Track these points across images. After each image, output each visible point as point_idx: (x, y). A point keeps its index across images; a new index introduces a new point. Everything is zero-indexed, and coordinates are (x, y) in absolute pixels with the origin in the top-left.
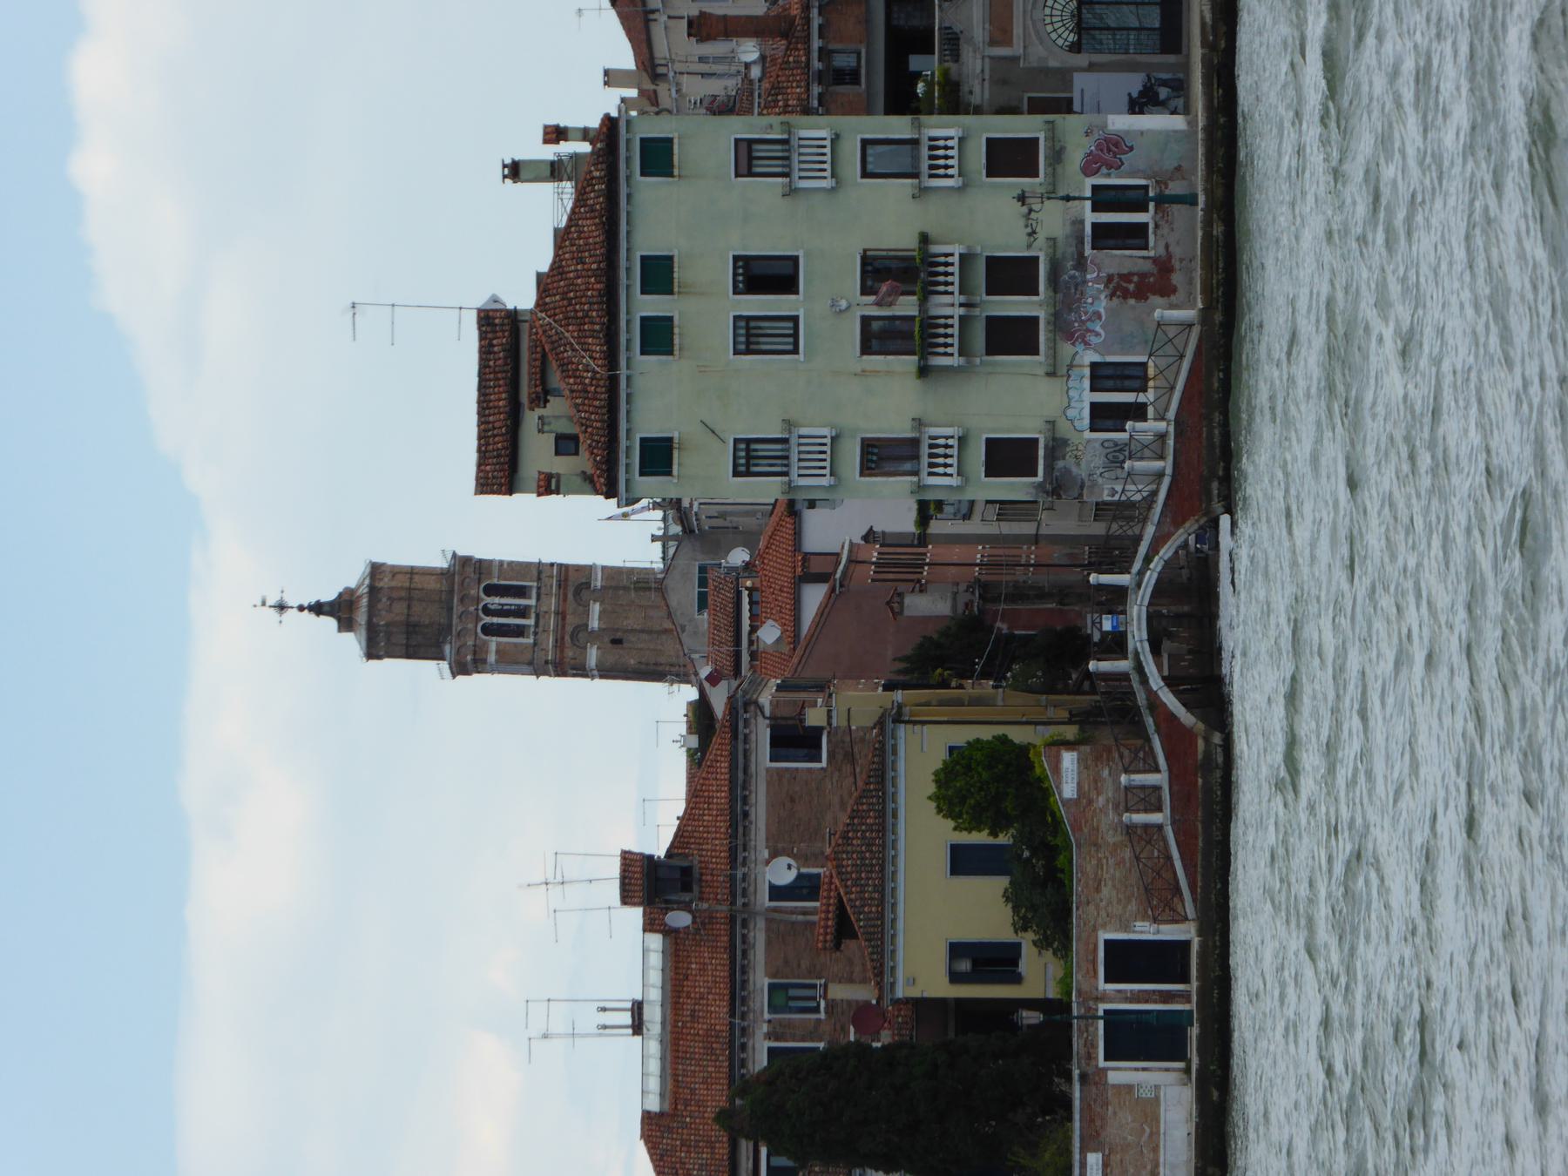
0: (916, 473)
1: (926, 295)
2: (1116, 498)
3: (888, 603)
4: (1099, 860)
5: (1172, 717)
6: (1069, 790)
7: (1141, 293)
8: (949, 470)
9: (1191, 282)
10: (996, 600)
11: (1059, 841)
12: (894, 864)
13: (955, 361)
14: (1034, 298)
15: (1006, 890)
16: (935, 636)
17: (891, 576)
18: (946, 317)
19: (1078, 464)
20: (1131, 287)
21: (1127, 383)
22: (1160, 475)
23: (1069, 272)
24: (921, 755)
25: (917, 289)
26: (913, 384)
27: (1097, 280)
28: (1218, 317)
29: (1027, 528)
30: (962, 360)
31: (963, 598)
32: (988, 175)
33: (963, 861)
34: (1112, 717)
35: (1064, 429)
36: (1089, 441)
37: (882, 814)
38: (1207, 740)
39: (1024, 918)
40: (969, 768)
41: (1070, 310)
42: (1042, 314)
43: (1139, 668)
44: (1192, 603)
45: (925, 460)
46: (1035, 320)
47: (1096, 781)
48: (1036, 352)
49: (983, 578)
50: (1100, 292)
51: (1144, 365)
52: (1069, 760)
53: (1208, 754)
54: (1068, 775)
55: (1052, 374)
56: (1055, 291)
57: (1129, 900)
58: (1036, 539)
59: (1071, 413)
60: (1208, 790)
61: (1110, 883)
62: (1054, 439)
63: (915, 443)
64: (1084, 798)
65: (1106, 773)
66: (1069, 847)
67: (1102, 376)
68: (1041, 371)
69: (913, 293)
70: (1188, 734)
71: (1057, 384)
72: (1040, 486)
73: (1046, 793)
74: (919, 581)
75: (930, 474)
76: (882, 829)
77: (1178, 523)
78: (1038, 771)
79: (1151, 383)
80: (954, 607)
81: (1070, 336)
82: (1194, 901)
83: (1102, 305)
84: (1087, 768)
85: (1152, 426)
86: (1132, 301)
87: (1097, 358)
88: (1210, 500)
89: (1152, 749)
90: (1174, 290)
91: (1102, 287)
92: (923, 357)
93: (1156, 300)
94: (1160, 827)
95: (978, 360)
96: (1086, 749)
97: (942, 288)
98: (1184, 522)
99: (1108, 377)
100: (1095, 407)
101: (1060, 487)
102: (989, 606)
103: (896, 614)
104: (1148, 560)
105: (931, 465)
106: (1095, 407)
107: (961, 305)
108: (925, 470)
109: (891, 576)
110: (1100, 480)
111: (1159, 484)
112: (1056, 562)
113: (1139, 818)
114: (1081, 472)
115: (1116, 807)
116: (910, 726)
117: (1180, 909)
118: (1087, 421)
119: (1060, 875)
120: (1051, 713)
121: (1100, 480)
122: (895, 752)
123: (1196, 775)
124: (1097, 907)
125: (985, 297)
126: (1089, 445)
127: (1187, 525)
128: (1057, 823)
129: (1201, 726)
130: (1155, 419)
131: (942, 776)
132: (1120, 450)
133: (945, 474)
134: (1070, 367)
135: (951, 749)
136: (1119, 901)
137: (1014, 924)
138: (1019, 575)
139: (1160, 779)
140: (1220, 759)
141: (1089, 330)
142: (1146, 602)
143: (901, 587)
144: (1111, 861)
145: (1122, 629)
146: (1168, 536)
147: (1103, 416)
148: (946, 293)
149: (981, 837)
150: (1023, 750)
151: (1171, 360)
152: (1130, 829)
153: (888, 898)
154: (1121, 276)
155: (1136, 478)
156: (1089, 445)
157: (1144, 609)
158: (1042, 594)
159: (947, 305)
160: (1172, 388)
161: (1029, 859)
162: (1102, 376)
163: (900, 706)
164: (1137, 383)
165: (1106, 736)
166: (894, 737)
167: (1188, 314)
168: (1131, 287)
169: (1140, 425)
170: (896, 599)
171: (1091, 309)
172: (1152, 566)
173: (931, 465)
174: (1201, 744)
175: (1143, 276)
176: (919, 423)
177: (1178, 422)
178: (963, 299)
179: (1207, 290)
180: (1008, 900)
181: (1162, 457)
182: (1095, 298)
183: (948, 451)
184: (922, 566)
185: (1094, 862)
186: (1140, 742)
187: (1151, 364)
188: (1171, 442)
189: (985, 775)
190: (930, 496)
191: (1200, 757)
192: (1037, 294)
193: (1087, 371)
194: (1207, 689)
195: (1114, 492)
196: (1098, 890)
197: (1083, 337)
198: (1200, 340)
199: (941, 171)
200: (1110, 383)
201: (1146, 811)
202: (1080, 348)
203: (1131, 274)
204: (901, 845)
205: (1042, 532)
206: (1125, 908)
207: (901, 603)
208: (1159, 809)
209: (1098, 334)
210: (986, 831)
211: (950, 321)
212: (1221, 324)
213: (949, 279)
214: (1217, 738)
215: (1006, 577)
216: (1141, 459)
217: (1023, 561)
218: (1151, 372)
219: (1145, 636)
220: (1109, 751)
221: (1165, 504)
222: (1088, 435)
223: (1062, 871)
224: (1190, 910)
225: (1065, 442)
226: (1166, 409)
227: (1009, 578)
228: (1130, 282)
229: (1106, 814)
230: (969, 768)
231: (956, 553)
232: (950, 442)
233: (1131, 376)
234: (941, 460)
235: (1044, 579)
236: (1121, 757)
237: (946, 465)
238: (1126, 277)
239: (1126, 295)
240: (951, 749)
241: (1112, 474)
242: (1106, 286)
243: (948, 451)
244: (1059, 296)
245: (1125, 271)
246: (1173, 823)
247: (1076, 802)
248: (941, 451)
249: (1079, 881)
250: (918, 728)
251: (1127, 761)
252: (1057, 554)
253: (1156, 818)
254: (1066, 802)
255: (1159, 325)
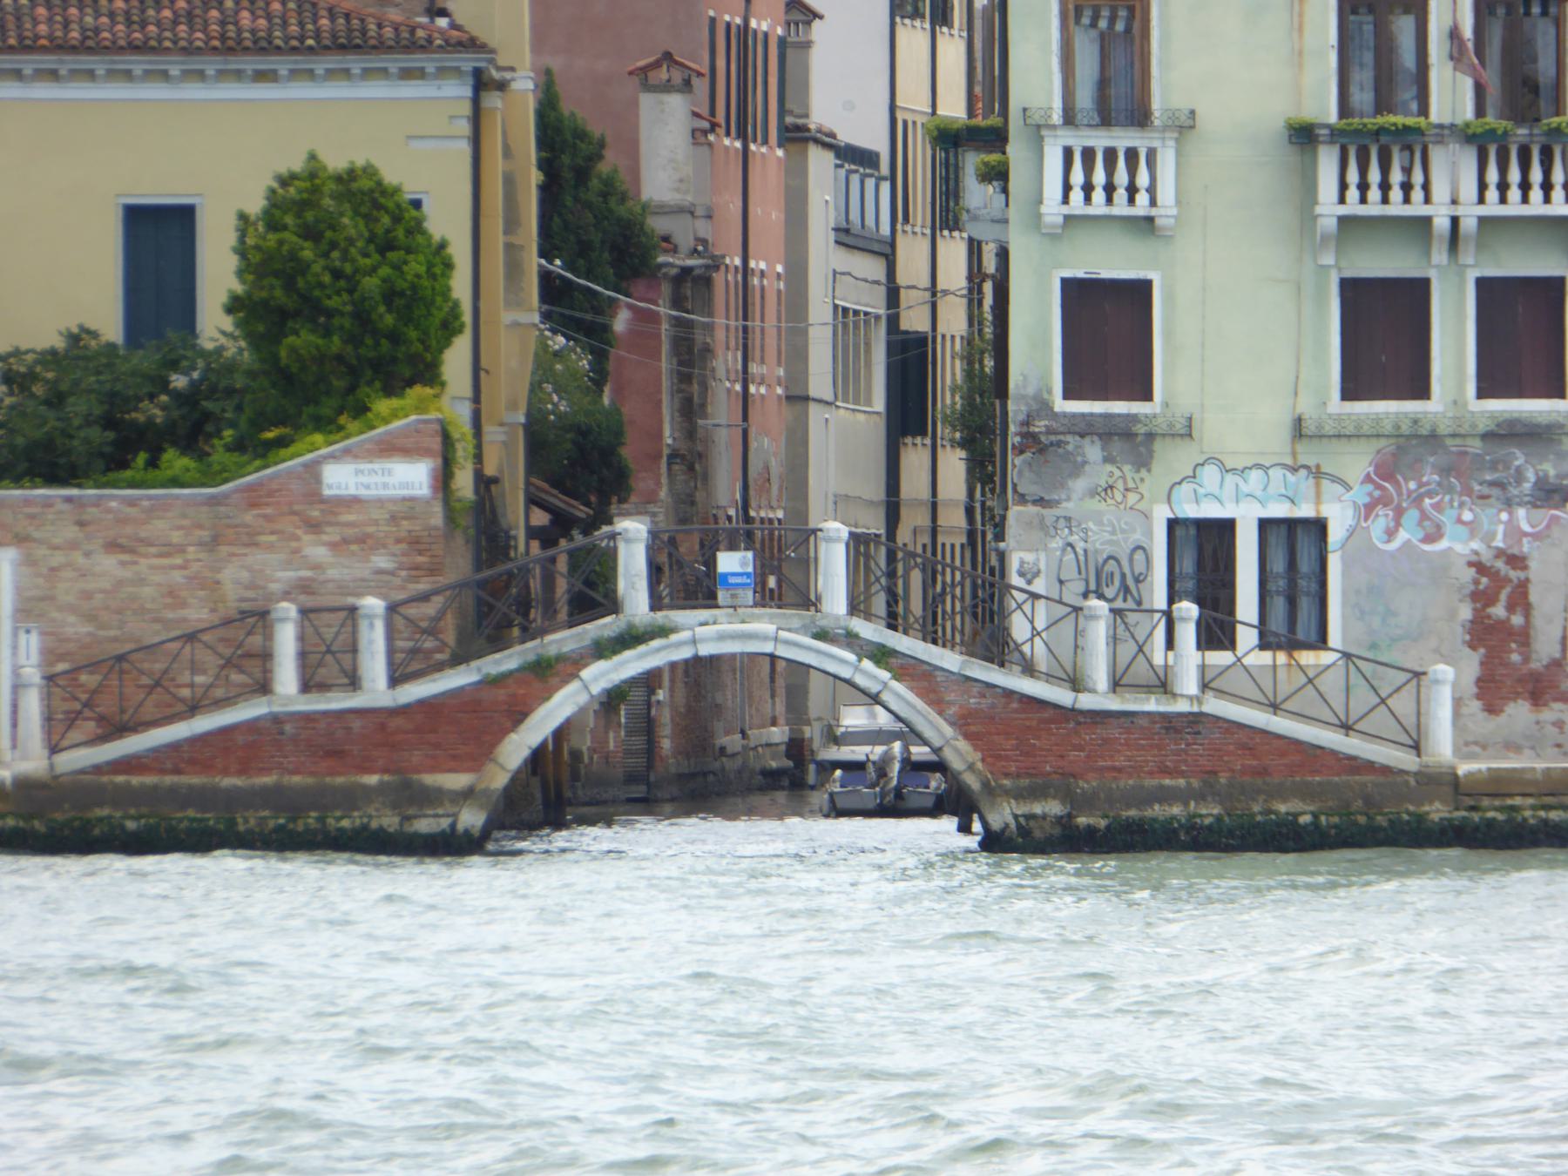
0: (1069, 119)
1: (1479, 141)
2: (1016, 580)
3: (668, 56)
4: (181, 549)
5: (518, 715)
6: (344, 476)
7: (1487, 635)
8: (1077, 195)
9: (1512, 747)
10: (677, 302)
11: (219, 456)
12: (149, 75)
13: (1328, 206)
14: (1471, 388)
15: (94, 334)
16: (603, 168)
17: (721, 63)
18: (1426, 187)
19: (1093, 493)
20: (1499, 611)
21: (1279, 605)
22: (1076, 683)
23: (1532, 468)
24: (411, 139)
25: (1491, 120)
26: (1276, 111)
27: (1514, 531)
28: (1437, 811)
29: (820, 382)
30: (1328, 224)
31: (683, 232)
32: (1066, 283)
33: (158, 238)
34: (515, 567)
35: (1172, 459)
36: (1147, 516)
37: (263, 46)
38: (468, 794)
39: (31, 376)
40: (386, 246)
41: (1445, 471)
42: (1434, 408)
43: (630, 639)
44: (696, 758)
45: (1100, 140)
46: (1421, 390)
47: (361, 540)
48: (1348, 394)
49: (718, 278)
50: (1488, 538)
51: (1321, 642)
52: (411, 477)
53: (430, 798)
54: (377, 475)
55: (1299, 430)
56: (1487, 436)
57: (91, 617)
58: (798, 399)
59: (1210, 474)
60: (352, 798)
61: (126, 573)
62: (1151, 436)
63: (1140, 117)
64: (324, 513)
65: (382, 561)
66: (210, 477)
67: (1295, 540)
68: (1306, 406)
69: (1480, 111)
70: (481, 751)
71: (1277, 441)
72: (1045, 407)
73: (328, 425)
74: (714, 126)
75: (1068, 153)
76: (230, 47)
77: (965, 723)
78: (383, 406)
79: (1282, 658)
80: (665, 210)
81: (1385, 471)
82: (98, 769)
83: (1458, 545)
84: (394, 519)
85: (1189, 660)
86: (1466, 612)
87: (1335, 534)
88: (1019, 795)
89: (439, 667)
90: (1492, 709)
91: (1499, 542)
92: (1335, 134)
93: (1472, 664)
94: (264, 687)
95: (1328, 259)
96: (437, 518)
97: (1492, 176)
98: (968, 736)
99: (1292, 564)
100: (1226, 528)
101: (1042, 450)
102: (666, 289)
103: (643, 77)
104: (882, 655)
105: (1089, 155)
106: (1226, 528)
107: (1455, 221)
108: (1078, 140)
109: (721, 63)
110: (1057, 543)
111: (1050, 677)
112: (753, 445)
113: (286, 640)
114: (1076, 498)
115: (305, 587)
116: (466, 109)
117: (75, 736)
118: (1191, 511)
119: (142, 458)
120: (492, 433)
121: (1057, 543)
122: (407, 74)
123: (385, 771)
124: (73, 545)
125: (1472, 276)
126: (1134, 520)
127: (963, 745)
128: (266, 451)
129: (498, 780)
130: (1203, 668)
131: (365, 184)
132: (1126, 590)
133: (1067, 188)
134: (1317, 473)
135: (417, 204)
136: (87, 595)
137: (17, 353)
138: (726, 361)
139: (376, 690)
140: (424, 826)
141: (1399, 513)
142: (782, 651)
143: (701, 86)
144: (178, 577)
145: (722, 596)
146: (938, 704)
147: (1205, 549)
148: (1482, 186)
149: (218, 274)
150: (427, 373)
151: (1338, 702)
152: (261, 618)
153: (67, 63)
154: (1522, 588)
155: (1067, 627)
156: (1134, 520)
157: (768, 648)
158: (691, 411)
159: (1453, 186)
160: (1275, 707)
161: (164, 385)
162: (1295, 540)
163: (502, 86)
164: (1278, 623)
165: (459, 565)
166: (442, 72)
167: (1443, 746)
168: (1499, 611)
169: (1187, 634)
170: (678, 76)
171: (1447, 518)
172: (867, 664)
173: (1089, 155)
174: (456, 781)
175: (1524, 637)
176: (1185, 126)
177: (1196, 721)
178: (1469, 225)
179: (1498, 785)
180: (74, 339)
181: (1116, 685)
182: (1472, 528)
183: (1121, 194)
184: (742, 135)
185: (176, 537)
186: (450, 637)
187: (1326, 658)
188: (1152, 704)
189: (371, 283)
190: (1016, 150)
191: (430, 779)
192: (1482, 394)
193: (1305, 511)
194: (555, 798)
195: (1029, 575)
196: (113, 546)
197: (1384, 501)
198: (1386, 770)
199: (1077, 177)
200: (1278, 565)
201: (303, 655)
202: (1361, 494)
203: (1527, 609)
204: (194, 92)
205: (813, 408)
206: (72, 609)
207: (667, 87)
208: (306, 686)
209: (1390, 534)
210: (239, 288)
211: (1417, 194)
212: (1420, 818)
213: (1374, 194)
214: (471, 819)
215: (722, 324)
216: (1114, 640)
217: (754, 368)
218: (1307, 658)
219: (705, 650)
220: (433, 571)
221: (1009, 694)
222: (1161, 514)
223: (153, 463)
224: (77, 759)
225: (1143, 461)
226: (1221, 693)
227: (720, 335)
228: (1511, 608)
229: (287, 565)
230: (386, 246)
231: (768, 214)
232: (1142, 198)
233: (1297, 615)
234: (1099, 177)
235: (721, 412)
236: (425, 597)
237: (1088, 188)
238: (1520, 599)
239: (1482, 598)
240: (417, 204)
241: (1070, 572)
242: (1500, 553)
243: (1121, 194)
244: (1475, 446)
245: (1533, 597)
246: (277, 720)
247: (314, 495)
248: (1122, 177)
249: (132, 502)
250: (464, 127)
251: (412, 611)
252: (768, 448)
253: (286, 677)
254: (313, 471)
255: (1418, 675)
